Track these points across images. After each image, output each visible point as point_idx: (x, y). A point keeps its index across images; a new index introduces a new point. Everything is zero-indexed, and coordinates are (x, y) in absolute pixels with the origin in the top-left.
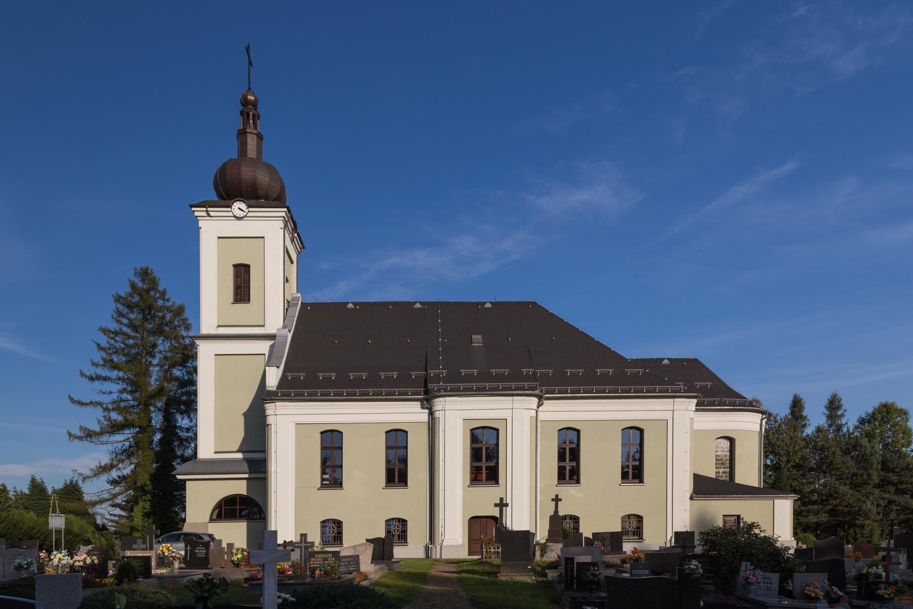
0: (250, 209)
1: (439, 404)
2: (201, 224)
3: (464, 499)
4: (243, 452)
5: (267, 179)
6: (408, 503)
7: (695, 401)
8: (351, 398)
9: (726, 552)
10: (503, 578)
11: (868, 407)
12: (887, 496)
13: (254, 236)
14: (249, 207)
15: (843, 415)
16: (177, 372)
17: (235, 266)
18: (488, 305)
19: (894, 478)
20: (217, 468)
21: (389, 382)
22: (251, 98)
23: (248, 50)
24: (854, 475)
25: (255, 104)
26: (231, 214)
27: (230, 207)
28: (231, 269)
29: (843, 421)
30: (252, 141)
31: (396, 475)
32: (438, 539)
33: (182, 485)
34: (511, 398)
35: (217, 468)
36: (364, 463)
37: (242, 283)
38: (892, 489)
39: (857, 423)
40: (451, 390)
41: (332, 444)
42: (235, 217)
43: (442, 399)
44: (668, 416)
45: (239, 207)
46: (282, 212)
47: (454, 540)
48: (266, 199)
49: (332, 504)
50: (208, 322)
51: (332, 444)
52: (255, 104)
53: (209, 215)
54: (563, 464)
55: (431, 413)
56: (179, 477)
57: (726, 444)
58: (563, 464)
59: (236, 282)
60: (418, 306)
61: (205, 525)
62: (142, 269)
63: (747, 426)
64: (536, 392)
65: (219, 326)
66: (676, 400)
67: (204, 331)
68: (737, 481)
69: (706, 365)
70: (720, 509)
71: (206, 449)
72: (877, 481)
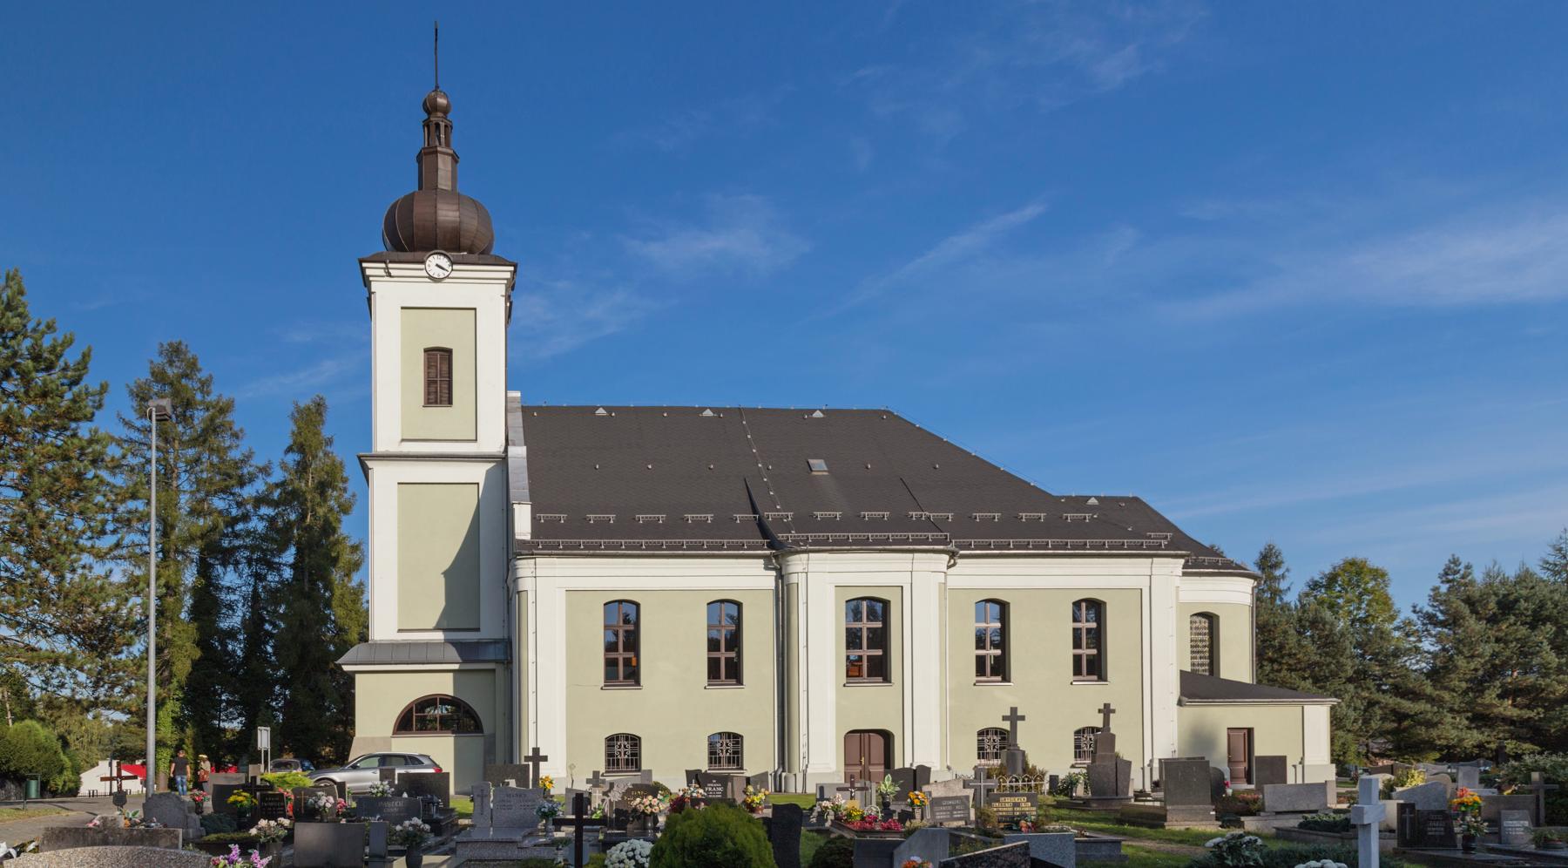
1: (798, 564)
3: (837, 703)
4: (444, 630)
5: (475, 223)
6: (746, 709)
8: (612, 552)
9: (1223, 782)
10: (1177, 828)
11: (1321, 568)
12: (1365, 694)
13: (410, 303)
14: (453, 263)
15: (1283, 576)
16: (219, 503)
17: (426, 351)
18: (818, 414)
20: (403, 655)
22: (442, 101)
24: (1317, 663)
25: (446, 111)
26: (424, 273)
27: (423, 262)
28: (421, 357)
29: (1283, 585)
30: (444, 164)
31: (725, 664)
32: (798, 764)
33: (350, 678)
34: (910, 556)
35: (403, 655)
37: (439, 377)
38: (1370, 683)
39: (1307, 589)
40: (815, 543)
42: (430, 277)
44: (1143, 583)
45: (436, 263)
46: (505, 272)
47: (822, 761)
48: (471, 252)
49: (624, 710)
50: (387, 434)
52: (446, 111)
54: (715, 655)
55: (781, 576)
56: (346, 668)
57: (1205, 623)
58: (715, 655)
59: (428, 374)
60: (708, 413)
61: (386, 741)
62: (170, 345)
63: (1232, 596)
64: (951, 547)
67: (381, 446)
69: (1152, 505)
70: (1225, 717)
71: (384, 626)
72: (1350, 673)
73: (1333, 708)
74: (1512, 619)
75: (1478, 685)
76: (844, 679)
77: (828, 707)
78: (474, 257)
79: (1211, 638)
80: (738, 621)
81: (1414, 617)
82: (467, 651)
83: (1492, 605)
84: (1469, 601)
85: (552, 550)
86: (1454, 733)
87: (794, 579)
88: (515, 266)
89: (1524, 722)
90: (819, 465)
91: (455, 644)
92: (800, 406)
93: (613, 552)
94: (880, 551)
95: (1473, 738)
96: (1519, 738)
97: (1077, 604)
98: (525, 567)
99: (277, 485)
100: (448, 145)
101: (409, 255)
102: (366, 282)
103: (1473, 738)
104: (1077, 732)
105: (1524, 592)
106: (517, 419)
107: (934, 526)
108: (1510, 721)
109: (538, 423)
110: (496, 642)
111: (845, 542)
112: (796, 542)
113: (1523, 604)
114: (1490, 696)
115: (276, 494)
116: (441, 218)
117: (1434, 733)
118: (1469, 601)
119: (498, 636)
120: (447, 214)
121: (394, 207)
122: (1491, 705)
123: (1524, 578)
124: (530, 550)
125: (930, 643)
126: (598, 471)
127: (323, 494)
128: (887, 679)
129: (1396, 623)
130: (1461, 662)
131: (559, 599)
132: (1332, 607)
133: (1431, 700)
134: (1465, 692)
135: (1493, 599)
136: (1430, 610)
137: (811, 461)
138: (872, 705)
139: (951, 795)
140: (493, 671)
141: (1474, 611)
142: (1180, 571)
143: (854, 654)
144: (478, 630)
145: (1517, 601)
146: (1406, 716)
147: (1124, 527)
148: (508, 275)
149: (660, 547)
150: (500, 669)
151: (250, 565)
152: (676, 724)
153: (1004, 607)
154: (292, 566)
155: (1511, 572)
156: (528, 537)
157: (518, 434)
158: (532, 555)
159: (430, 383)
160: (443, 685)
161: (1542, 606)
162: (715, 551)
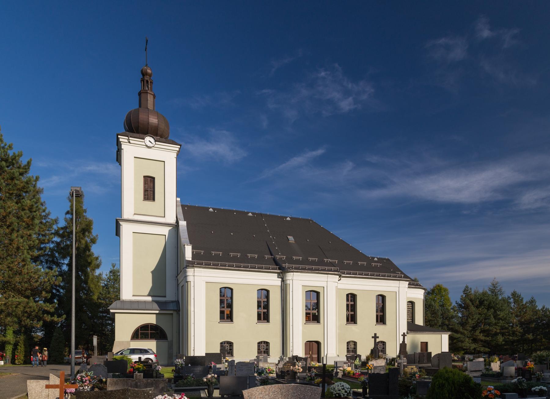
0: (157, 143)
2: (123, 146)
3: (303, 331)
4: (152, 296)
6: (270, 332)
7: (408, 283)
13: (146, 158)
14: (156, 141)
17: (144, 177)
19: (447, 322)
20: (134, 306)
21: (252, 260)
22: (149, 71)
24: (431, 320)
25: (150, 75)
27: (144, 139)
30: (150, 98)
31: (264, 316)
35: (134, 306)
36: (245, 307)
41: (352, 298)
42: (146, 146)
43: (292, 273)
44: (396, 290)
45: (149, 140)
46: (177, 148)
48: (161, 137)
49: (227, 332)
50: (128, 211)
51: (352, 298)
53: (129, 142)
56: (112, 311)
59: (145, 187)
61: (128, 343)
63: (418, 295)
65: (135, 214)
66: (401, 282)
68: (416, 323)
71: (127, 293)
73: (449, 335)
74: (483, 307)
75: (474, 328)
78: (163, 139)
79: (412, 309)
80: (268, 297)
81: (456, 305)
82: (162, 305)
83: (477, 302)
84: (471, 300)
86: (468, 345)
87: (288, 282)
88: (181, 146)
89: (485, 341)
90: (291, 238)
91: (157, 302)
92: (282, 215)
93: (223, 267)
94: (317, 273)
95: (473, 346)
96: (484, 346)
97: (347, 295)
98: (190, 272)
99: (62, 228)
100: (151, 90)
101: (138, 135)
102: (119, 144)
103: (473, 346)
105: (486, 298)
106: (180, 209)
107: (332, 264)
108: (482, 341)
109: (188, 211)
110: (172, 302)
111: (305, 269)
112: (289, 268)
113: (485, 302)
114: (477, 333)
115: (61, 232)
116: (150, 121)
117: (463, 344)
118: (471, 300)
119: (174, 299)
120: (153, 120)
121: (130, 113)
122: (478, 335)
123: (484, 294)
124: (191, 264)
125: (333, 309)
126: (218, 233)
127: (84, 234)
128: (318, 322)
129: (451, 307)
130: (470, 320)
131: (203, 284)
132: (434, 300)
133: (462, 333)
134: (471, 331)
135: (478, 300)
136: (460, 303)
138: (314, 332)
139: (378, 365)
140: (172, 314)
141: (473, 304)
142: (407, 286)
143: (348, 313)
144: (165, 297)
145: (484, 301)
146: (455, 339)
147: (386, 269)
148: (178, 149)
150: (175, 314)
151: (47, 263)
152: (246, 338)
154: (67, 265)
155: (481, 291)
156: (190, 259)
157: (181, 216)
158: (193, 267)
159: (146, 191)
160: (151, 319)
161: (490, 303)
162: (260, 269)
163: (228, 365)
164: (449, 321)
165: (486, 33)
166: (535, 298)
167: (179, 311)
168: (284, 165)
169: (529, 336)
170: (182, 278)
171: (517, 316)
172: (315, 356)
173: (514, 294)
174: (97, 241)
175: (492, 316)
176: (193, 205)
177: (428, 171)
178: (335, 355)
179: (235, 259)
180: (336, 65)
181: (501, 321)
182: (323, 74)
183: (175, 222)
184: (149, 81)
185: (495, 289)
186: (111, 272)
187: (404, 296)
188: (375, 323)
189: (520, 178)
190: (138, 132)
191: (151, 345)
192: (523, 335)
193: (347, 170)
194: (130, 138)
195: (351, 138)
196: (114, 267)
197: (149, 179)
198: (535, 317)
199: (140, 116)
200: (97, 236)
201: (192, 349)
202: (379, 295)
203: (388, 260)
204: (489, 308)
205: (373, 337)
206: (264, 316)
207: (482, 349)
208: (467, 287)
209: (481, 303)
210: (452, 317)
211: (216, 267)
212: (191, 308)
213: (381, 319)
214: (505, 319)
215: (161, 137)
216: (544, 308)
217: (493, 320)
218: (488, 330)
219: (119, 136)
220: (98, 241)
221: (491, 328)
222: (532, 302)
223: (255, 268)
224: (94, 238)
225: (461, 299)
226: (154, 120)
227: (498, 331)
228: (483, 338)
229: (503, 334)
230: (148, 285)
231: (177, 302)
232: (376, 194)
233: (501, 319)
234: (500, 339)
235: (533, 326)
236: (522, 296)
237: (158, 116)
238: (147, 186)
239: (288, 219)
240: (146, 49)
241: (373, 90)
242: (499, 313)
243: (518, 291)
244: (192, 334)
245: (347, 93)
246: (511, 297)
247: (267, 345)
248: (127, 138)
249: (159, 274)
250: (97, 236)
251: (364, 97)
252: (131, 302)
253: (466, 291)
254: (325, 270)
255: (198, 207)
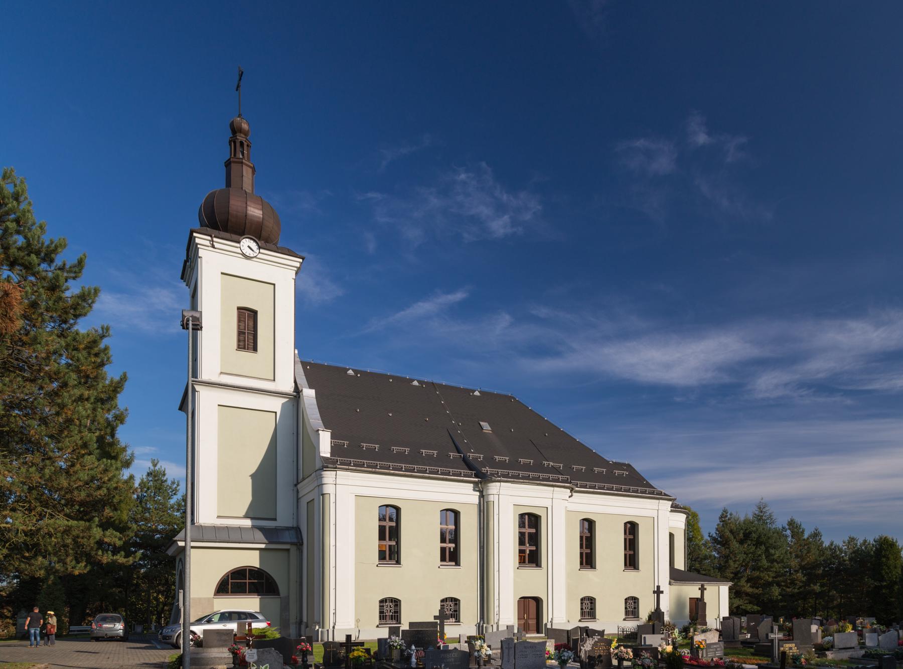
0: (262, 251)
1: (494, 489)
2: (201, 253)
4: (252, 519)
6: (461, 582)
7: (670, 503)
13: (237, 275)
14: (260, 248)
17: (239, 308)
20: (220, 536)
21: (429, 461)
22: (245, 126)
23: (241, 75)
25: (246, 134)
26: (238, 250)
27: (239, 242)
30: (247, 172)
31: (451, 555)
32: (493, 619)
34: (552, 488)
35: (220, 536)
36: (420, 539)
41: (589, 527)
42: (243, 254)
45: (247, 244)
46: (296, 262)
47: (506, 615)
50: (209, 368)
51: (589, 527)
53: (213, 246)
54: (523, 548)
58: (523, 548)
59: (239, 326)
61: (210, 602)
63: (679, 521)
65: (221, 373)
66: (556, 489)
71: (208, 511)
76: (518, 565)
77: (510, 582)
82: (271, 534)
83: (741, 535)
84: (731, 531)
85: (347, 466)
87: (491, 498)
88: (303, 259)
90: (486, 426)
91: (262, 529)
94: (538, 484)
98: (329, 477)
100: (249, 160)
104: (381, 601)
106: (300, 366)
107: (555, 470)
108: (747, 594)
109: (313, 371)
111: (517, 477)
112: (492, 475)
114: (743, 582)
116: (249, 212)
120: (255, 212)
122: (744, 586)
124: (330, 464)
126: (371, 412)
129: (703, 542)
131: (351, 499)
135: (742, 532)
136: (714, 535)
137: (482, 423)
138: (532, 582)
140: (288, 550)
142: (669, 509)
144: (275, 519)
147: (630, 482)
149: (362, 466)
150: (293, 549)
153: (456, 514)
156: (328, 455)
157: (303, 381)
158: (335, 469)
159: (240, 333)
160: (251, 559)
162: (445, 476)
163: (670, 655)
164: (700, 562)
165: (702, 139)
166: (820, 530)
167: (302, 544)
168: (402, 313)
169: (815, 588)
170: (312, 487)
171: (797, 556)
172: (533, 622)
173: (791, 523)
174: (127, 419)
175: (764, 557)
176: (319, 362)
177: (625, 335)
178: (564, 620)
179: (400, 458)
180: (484, 164)
181: (775, 564)
182: (463, 176)
183: (292, 390)
184: (245, 144)
185: (762, 515)
186: (149, 474)
187: (662, 524)
188: (377, 562)
189: (754, 352)
190: (226, 230)
191: (250, 603)
192: (807, 584)
193: (500, 327)
194: (215, 239)
195: (506, 277)
196: (155, 465)
197: (247, 313)
198: (822, 558)
199: (232, 202)
200: (126, 410)
201: (332, 611)
202: (584, 520)
203: (629, 466)
204: (758, 543)
205: (662, 592)
206: (451, 555)
207: (749, 607)
208: (725, 511)
209: (747, 535)
210: (706, 558)
211: (373, 469)
212: (330, 540)
213: (631, 562)
214: (782, 561)
215: (267, 241)
216: (832, 544)
217: (765, 563)
218: (759, 578)
219: (195, 234)
220: (128, 420)
221: (762, 575)
222: (816, 534)
223: (437, 473)
224: (122, 414)
225: (717, 529)
226: (256, 211)
227: (770, 579)
228: (750, 590)
229: (779, 585)
230: (244, 497)
231: (297, 530)
232: (547, 365)
233: (776, 561)
234: (776, 591)
235: (821, 572)
236: (803, 526)
237: (264, 206)
238: (242, 324)
239: (477, 393)
240: (238, 86)
241: (540, 207)
242: (772, 551)
243: (798, 520)
244: (332, 586)
245: (500, 208)
246: (787, 527)
247: (456, 604)
248: (209, 238)
249: (264, 479)
250: (126, 410)
251: (528, 217)
252: (215, 529)
253: (724, 518)
254: (548, 480)
255: (329, 367)
